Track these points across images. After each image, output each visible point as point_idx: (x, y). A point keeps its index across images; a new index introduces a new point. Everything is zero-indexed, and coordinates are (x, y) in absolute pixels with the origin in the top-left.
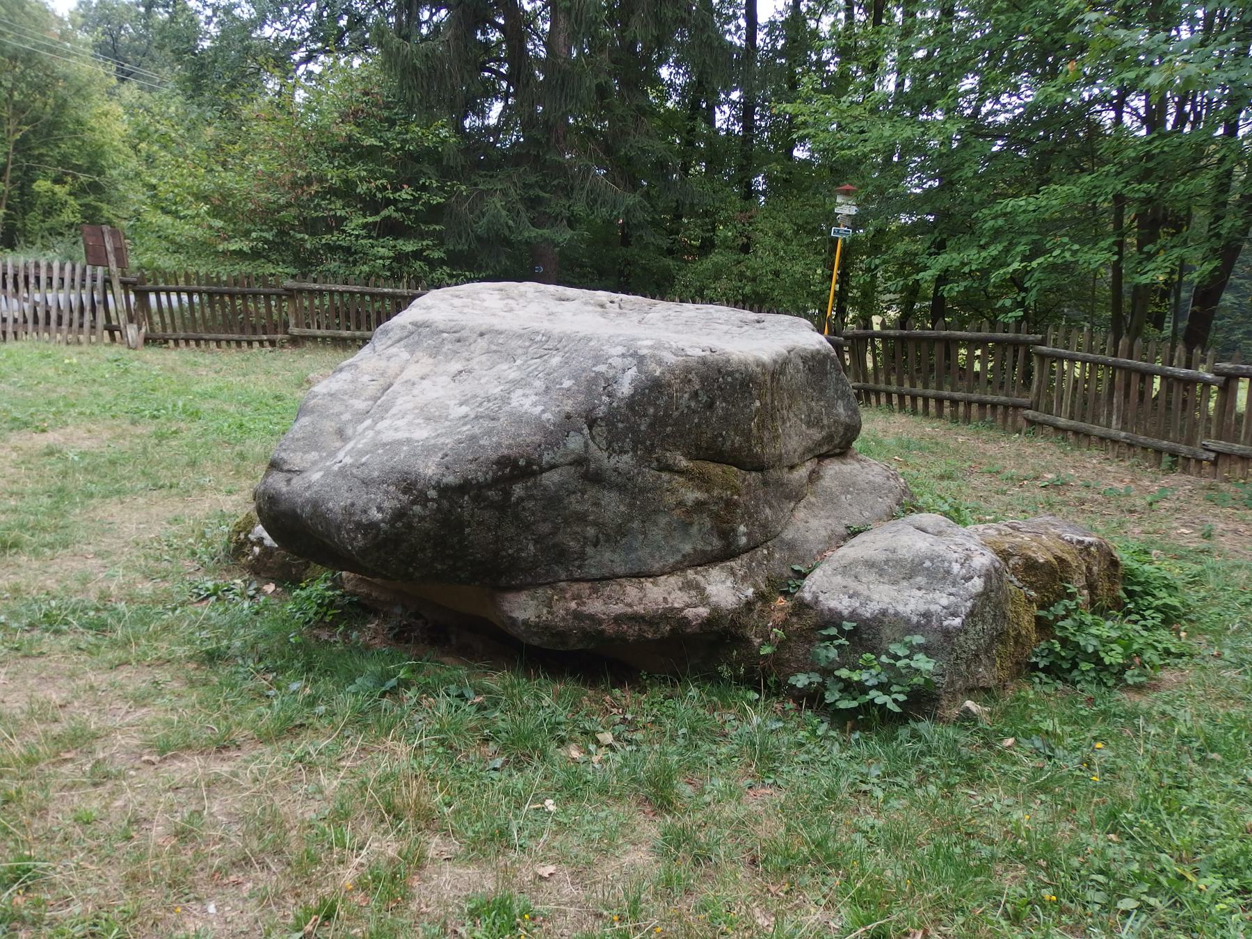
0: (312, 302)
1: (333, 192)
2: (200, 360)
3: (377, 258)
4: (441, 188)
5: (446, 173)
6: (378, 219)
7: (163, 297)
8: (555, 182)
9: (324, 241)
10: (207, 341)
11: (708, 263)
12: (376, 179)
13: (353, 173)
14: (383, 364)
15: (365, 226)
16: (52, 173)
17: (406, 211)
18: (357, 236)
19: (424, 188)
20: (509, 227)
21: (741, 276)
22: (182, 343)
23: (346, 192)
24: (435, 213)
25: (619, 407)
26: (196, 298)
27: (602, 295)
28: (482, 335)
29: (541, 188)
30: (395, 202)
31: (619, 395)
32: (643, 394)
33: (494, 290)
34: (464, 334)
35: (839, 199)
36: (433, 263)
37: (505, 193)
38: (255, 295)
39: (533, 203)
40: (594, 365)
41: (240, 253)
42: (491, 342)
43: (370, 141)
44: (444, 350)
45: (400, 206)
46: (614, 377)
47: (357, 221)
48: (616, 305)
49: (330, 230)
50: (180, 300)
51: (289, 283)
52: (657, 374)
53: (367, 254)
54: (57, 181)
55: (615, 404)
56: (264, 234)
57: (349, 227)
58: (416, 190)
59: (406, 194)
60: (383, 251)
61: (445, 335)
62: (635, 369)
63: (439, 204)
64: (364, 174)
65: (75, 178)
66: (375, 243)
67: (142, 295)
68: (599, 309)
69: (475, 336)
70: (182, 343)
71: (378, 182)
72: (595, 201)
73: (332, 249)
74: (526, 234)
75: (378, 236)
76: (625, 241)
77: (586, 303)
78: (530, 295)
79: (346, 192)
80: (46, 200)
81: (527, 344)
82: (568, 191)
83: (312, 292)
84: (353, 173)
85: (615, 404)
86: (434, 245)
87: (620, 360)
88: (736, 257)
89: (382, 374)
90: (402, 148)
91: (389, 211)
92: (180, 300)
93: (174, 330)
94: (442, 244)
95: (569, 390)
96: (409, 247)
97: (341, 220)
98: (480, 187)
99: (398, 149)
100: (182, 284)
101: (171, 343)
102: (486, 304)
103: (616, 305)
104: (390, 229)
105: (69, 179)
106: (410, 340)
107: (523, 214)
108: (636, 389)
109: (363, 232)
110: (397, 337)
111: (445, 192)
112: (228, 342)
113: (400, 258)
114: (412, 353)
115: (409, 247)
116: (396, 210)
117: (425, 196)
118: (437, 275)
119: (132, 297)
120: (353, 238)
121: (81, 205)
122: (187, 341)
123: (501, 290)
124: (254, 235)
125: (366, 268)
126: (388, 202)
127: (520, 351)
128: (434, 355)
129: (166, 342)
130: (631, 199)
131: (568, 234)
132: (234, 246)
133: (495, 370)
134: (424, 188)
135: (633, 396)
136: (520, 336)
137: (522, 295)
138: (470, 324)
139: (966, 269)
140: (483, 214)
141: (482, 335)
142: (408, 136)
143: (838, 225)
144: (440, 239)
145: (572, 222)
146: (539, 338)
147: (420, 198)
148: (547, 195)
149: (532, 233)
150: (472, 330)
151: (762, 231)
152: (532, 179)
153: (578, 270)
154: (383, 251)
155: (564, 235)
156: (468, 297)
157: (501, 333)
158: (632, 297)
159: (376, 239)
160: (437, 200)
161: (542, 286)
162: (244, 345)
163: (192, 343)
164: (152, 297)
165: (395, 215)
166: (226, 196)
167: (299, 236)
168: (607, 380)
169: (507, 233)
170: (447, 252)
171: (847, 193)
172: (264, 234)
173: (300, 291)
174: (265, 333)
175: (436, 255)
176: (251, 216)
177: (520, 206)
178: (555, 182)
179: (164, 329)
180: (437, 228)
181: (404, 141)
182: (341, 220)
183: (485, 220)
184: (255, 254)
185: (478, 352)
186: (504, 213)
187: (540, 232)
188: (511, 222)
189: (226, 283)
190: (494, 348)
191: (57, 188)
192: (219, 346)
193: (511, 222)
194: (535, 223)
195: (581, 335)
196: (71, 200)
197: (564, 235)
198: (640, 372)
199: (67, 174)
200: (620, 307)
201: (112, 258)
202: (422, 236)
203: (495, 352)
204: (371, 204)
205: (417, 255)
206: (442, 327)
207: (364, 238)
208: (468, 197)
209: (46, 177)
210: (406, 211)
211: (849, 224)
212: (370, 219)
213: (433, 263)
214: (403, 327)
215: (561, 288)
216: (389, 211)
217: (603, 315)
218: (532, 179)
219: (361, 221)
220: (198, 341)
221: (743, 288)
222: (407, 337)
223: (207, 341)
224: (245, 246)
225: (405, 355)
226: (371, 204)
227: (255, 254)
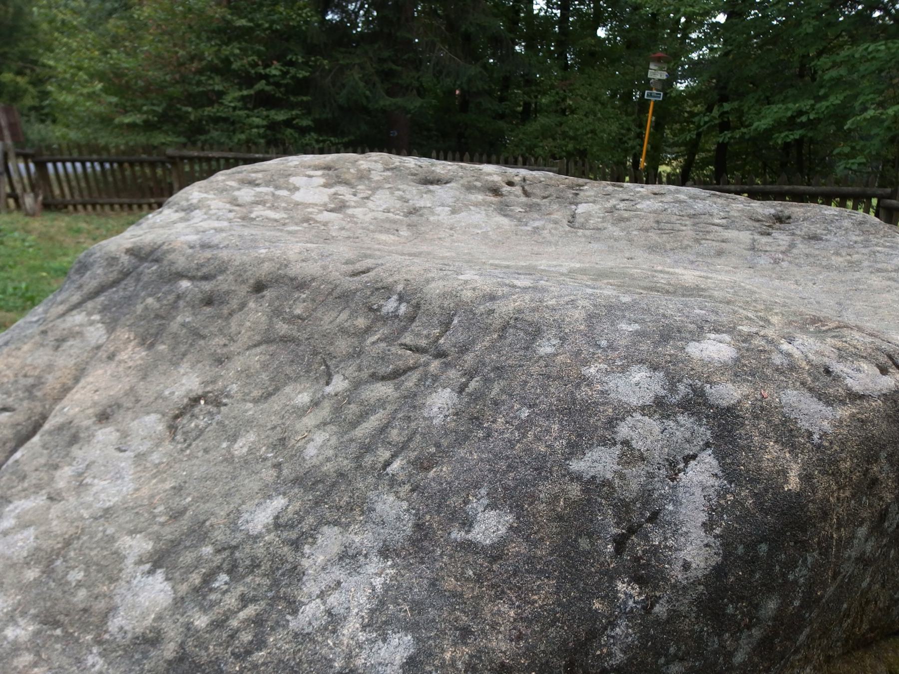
0: (192, 168)
1: (214, 69)
2: (83, 225)
3: (251, 126)
4: (306, 63)
5: (311, 50)
6: (252, 92)
7: (59, 165)
8: (405, 57)
9: (206, 113)
10: (102, 205)
11: (533, 126)
12: (247, 56)
13: (226, 51)
14: (42, 357)
15: (243, 98)
16: (14, 66)
17: (277, 85)
18: (235, 108)
19: (291, 64)
20: (367, 97)
21: (565, 135)
22: (80, 207)
23: (223, 69)
24: (302, 86)
25: (674, 615)
26: (107, 166)
27: (492, 172)
28: (259, 288)
29: (394, 62)
30: (266, 77)
31: (677, 574)
32: (751, 562)
33: (316, 168)
34: (223, 283)
35: (652, 66)
36: (303, 131)
37: (362, 67)
38: (142, 163)
39: (386, 75)
40: (575, 449)
41: (132, 126)
42: (277, 312)
43: (243, 22)
44: (174, 326)
45: (271, 80)
46: (646, 495)
47: (233, 96)
48: (517, 190)
49: (211, 103)
50: (93, 167)
51: (170, 151)
52: (793, 483)
53: (244, 124)
54: (20, 73)
55: (660, 609)
56: (156, 108)
57: (227, 100)
58: (284, 65)
59: (275, 70)
60: (257, 121)
61: (185, 284)
62: (708, 459)
63: (305, 77)
64: (237, 51)
65: (33, 70)
66: (250, 113)
67: (41, 166)
68: (492, 199)
69: (243, 290)
70: (80, 207)
71: (250, 59)
72: (440, 72)
73: (216, 120)
74: (382, 103)
75: (255, 108)
76: (464, 106)
77: (470, 188)
78: (376, 176)
79: (223, 69)
80: (11, 89)
81: (361, 322)
82: (417, 64)
83: (191, 159)
84: (226, 51)
85: (660, 609)
86: (303, 114)
87: (653, 424)
88: (559, 119)
89: (30, 390)
90: (270, 28)
91: (261, 85)
92: (93, 167)
93: (90, 195)
94: (309, 113)
95: (496, 553)
96: (280, 116)
97: (220, 94)
98: (341, 62)
99: (267, 29)
100: (75, 155)
101: (71, 208)
102: (298, 197)
103: (517, 190)
104: (264, 101)
105: (28, 71)
106: (116, 294)
107: (379, 85)
108: (727, 543)
109: (239, 104)
110: (94, 284)
111: (310, 66)
112: (121, 205)
113: (273, 126)
114: (111, 326)
115: (280, 116)
116: (268, 84)
117: (293, 70)
118: (307, 139)
119: (32, 166)
120: (231, 109)
121: (39, 92)
122: (85, 206)
123: (328, 168)
124: (145, 108)
125: (243, 137)
126: (261, 77)
127: (343, 345)
128: (148, 341)
129: (66, 207)
130: (473, 70)
131: (419, 102)
132: (127, 120)
133: (276, 403)
134: (291, 64)
135: (719, 572)
136: (345, 298)
137: (363, 176)
138: (238, 258)
139: (804, 119)
140: (343, 86)
141: (259, 288)
142: (275, 17)
143: (651, 89)
144: (307, 109)
145: (421, 92)
146: (390, 305)
147: (288, 72)
148: (399, 68)
149: (386, 102)
150: (240, 276)
151: (581, 96)
152: (386, 54)
153: (425, 133)
154: (257, 121)
155: (414, 103)
156: (267, 184)
157: (301, 285)
158: (537, 174)
159: (252, 110)
160: (302, 74)
161: (396, 160)
162: (135, 207)
163: (89, 207)
164: (50, 166)
165: (268, 88)
166: (118, 73)
167: (185, 109)
168: (623, 508)
169: (365, 102)
170: (314, 121)
171: (658, 60)
172: (156, 108)
173: (182, 158)
174: (152, 197)
175: (305, 122)
176: (145, 92)
177: (376, 79)
178: (405, 57)
179: (72, 195)
180: (305, 98)
181: (273, 22)
182: (220, 94)
183: (344, 92)
184: (148, 126)
185: (244, 338)
186: (362, 84)
187: (394, 100)
188: (368, 93)
189: (124, 153)
190: (282, 328)
191: (19, 79)
192: (112, 209)
193: (368, 93)
194: (390, 93)
195: (505, 308)
196: (31, 89)
197: (414, 103)
198: (730, 473)
199: (26, 68)
200: (526, 194)
201: (6, 133)
202: (292, 106)
203: (285, 340)
204: (247, 80)
205: (288, 123)
206: (181, 263)
207: (240, 109)
208: (330, 71)
209: (10, 70)
210: (277, 85)
211: (660, 87)
212: (245, 93)
213: (303, 131)
214: (112, 260)
215: (425, 162)
216: (261, 85)
217: (504, 209)
218: (386, 54)
219: (237, 94)
220: (94, 205)
221: (566, 146)
222: (115, 283)
223: (102, 205)
224: (138, 118)
225: (96, 333)
226: (247, 80)
227: (148, 126)
